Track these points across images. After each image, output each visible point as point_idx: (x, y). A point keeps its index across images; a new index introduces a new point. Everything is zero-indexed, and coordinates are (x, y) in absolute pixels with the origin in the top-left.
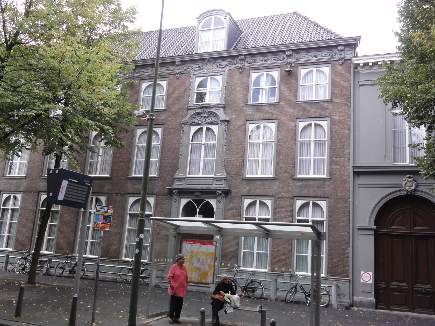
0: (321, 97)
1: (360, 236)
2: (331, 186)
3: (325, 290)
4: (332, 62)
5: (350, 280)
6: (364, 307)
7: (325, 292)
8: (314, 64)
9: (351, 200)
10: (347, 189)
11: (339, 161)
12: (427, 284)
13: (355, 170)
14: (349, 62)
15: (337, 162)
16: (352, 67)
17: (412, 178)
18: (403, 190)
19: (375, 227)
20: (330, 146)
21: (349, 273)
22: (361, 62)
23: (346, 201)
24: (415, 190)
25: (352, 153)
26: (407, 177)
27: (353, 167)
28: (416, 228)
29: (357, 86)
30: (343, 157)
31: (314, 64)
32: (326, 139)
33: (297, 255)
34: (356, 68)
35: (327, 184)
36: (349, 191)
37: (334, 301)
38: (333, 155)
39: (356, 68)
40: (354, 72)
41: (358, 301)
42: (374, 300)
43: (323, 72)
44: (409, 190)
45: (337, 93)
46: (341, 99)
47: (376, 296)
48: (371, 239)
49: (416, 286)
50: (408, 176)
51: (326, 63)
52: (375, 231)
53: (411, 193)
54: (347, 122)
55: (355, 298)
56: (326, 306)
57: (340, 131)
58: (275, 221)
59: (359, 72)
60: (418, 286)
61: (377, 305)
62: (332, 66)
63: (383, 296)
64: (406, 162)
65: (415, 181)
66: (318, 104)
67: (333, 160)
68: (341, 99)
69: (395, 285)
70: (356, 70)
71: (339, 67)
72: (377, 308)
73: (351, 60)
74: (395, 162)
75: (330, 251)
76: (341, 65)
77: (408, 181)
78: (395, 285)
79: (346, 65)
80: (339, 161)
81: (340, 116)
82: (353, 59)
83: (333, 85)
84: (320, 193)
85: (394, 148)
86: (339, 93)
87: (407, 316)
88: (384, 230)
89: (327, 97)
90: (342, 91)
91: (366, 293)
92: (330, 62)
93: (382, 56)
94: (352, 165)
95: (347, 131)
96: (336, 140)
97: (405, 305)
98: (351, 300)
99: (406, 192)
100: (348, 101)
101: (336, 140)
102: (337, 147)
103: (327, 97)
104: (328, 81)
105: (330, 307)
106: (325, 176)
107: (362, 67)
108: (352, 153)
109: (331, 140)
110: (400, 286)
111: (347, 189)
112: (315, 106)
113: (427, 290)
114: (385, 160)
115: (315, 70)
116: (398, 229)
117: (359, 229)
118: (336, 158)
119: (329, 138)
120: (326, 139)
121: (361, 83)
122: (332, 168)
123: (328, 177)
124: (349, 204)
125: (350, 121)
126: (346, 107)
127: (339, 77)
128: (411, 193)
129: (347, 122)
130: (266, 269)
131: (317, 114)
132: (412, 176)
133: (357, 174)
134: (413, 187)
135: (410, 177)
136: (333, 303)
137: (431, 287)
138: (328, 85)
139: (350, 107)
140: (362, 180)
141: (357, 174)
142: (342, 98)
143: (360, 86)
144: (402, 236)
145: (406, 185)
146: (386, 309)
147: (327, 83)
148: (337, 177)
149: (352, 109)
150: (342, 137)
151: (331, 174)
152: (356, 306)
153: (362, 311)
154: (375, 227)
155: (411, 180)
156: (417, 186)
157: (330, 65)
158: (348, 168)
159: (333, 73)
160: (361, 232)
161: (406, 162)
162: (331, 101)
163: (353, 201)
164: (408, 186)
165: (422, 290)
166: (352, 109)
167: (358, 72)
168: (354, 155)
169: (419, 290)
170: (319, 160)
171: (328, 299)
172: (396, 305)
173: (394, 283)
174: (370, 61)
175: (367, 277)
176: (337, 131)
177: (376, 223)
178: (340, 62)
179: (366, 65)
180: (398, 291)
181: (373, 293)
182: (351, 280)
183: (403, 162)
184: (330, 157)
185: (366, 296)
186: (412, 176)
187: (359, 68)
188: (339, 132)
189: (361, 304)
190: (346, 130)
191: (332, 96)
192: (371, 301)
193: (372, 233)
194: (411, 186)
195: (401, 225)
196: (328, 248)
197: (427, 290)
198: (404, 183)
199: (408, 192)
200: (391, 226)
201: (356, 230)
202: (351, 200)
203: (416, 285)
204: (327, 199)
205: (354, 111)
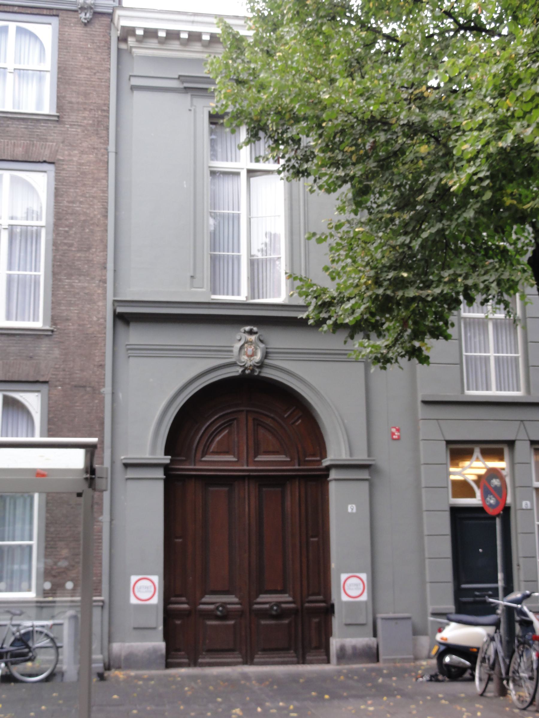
0: (29, 107)
1: (129, 483)
2: (57, 352)
3: (47, 636)
4: (60, 13)
5: (103, 601)
6: (138, 668)
7: (45, 642)
8: (11, 9)
9: (107, 390)
10: (97, 359)
11: (77, 284)
12: (283, 591)
13: (120, 310)
14: (105, 20)
15: (72, 286)
16: (115, 34)
17: (256, 333)
18: (234, 364)
19: (167, 460)
20: (55, 244)
21: (100, 582)
22: (140, 25)
23: (95, 392)
24: (261, 365)
25: (110, 265)
26: (245, 332)
27: (115, 301)
28: (260, 458)
29: (126, 88)
30: (88, 275)
31: (11, 9)
32: (43, 223)
33: (31, 539)
34: (123, 39)
35: (44, 345)
36: (102, 366)
37: (68, 664)
38: (62, 267)
39: (123, 39)
40: (119, 50)
41: (124, 654)
42: (162, 645)
43: (36, 37)
44: (249, 363)
45: (74, 100)
46: (85, 118)
47: (167, 637)
48: (158, 490)
49: (259, 600)
50: (247, 328)
51: (45, 12)
52: (167, 468)
53: (253, 371)
54: (98, 180)
55: (116, 647)
56: (47, 679)
57: (81, 203)
58: (51, 434)
59: (131, 52)
60: (263, 598)
61: (170, 660)
62: (62, 24)
63: (185, 634)
64: (239, 294)
65: (262, 341)
66: (23, 125)
67: (60, 280)
68: (85, 118)
69: (211, 601)
70: (123, 46)
71: (80, 30)
72: (168, 665)
73: (110, 15)
74: (214, 293)
75: (52, 529)
76: (85, 25)
77: (246, 342)
78: (211, 601)
79: (98, 26)
80: (77, 284)
81: (81, 164)
82: (118, 12)
83: (64, 76)
84: (25, 371)
85: (214, 259)
86: (80, 100)
87: (246, 677)
88: (188, 467)
89: (48, 108)
90: (86, 95)
91: (142, 630)
92: (55, 12)
93: (192, 18)
94: (110, 298)
95: (98, 206)
96: (70, 226)
97: (286, 649)
98: (106, 653)
99: (240, 370)
100: (100, 125)
101: (70, 226)
102: (71, 245)
103: (48, 108)
104: (48, 63)
105: (58, 678)
106: (38, 324)
107: (141, 40)
108: (110, 265)
109: (56, 225)
110: (224, 605)
111: (97, 359)
112: (13, 127)
113: (229, 606)
114: (192, 286)
115: (12, 27)
116: (217, 461)
117: (127, 466)
118: (69, 276)
119: (52, 220)
120: (43, 223)
121: (135, 82)
122: (59, 304)
123: (47, 327)
124: (102, 401)
125: (106, 178)
126: (94, 140)
127: (80, 57)
128: (253, 371)
129: (98, 180)
130: (29, 590)
131: (19, 152)
132: (255, 329)
133: (123, 319)
134: (258, 357)
135: (251, 332)
136: (65, 667)
137: (290, 599)
138: (48, 76)
139: (107, 142)
140: (136, 336)
141: (123, 319)
142: (86, 114)
143: (134, 88)
144: (227, 480)
145: (241, 351)
146: (188, 665)
147: (48, 68)
148: (72, 327)
149: (112, 147)
150: (85, 221)
151: (54, 320)
152: (119, 668)
153: (138, 678)
154: (167, 460)
155: (253, 338)
156: (266, 355)
157: (55, 21)
158: (100, 304)
159: (63, 44)
160: (132, 473)
161: (239, 294)
162: (58, 120)
163: (113, 393)
164: (246, 354)
165: (271, 608)
166: (112, 147)
167: (129, 51)
168: (115, 271)
169: (266, 610)
170: (22, 281)
171: (53, 657)
172: (211, 651)
173: (207, 598)
174: (163, 26)
175: (146, 590)
176: (73, 202)
177: (170, 447)
178: (83, 15)
179: (151, 34)
180: (218, 618)
181: (161, 628)
182: (107, 601)
183: (233, 294)
184: (54, 274)
185: (144, 639)
186: (255, 329)
187: (131, 41)
188: (77, 207)
189: (130, 661)
190: (96, 201)
191: (59, 108)
192: (155, 650)
193: (160, 474)
194: (254, 354)
195: (227, 453)
196: (47, 519)
197: (229, 606)
198: (238, 345)
199: (246, 368)
200: (203, 457)
201: (119, 467)
202: (107, 390)
203: (257, 597)
204: (45, 388)
205: (116, 153)
